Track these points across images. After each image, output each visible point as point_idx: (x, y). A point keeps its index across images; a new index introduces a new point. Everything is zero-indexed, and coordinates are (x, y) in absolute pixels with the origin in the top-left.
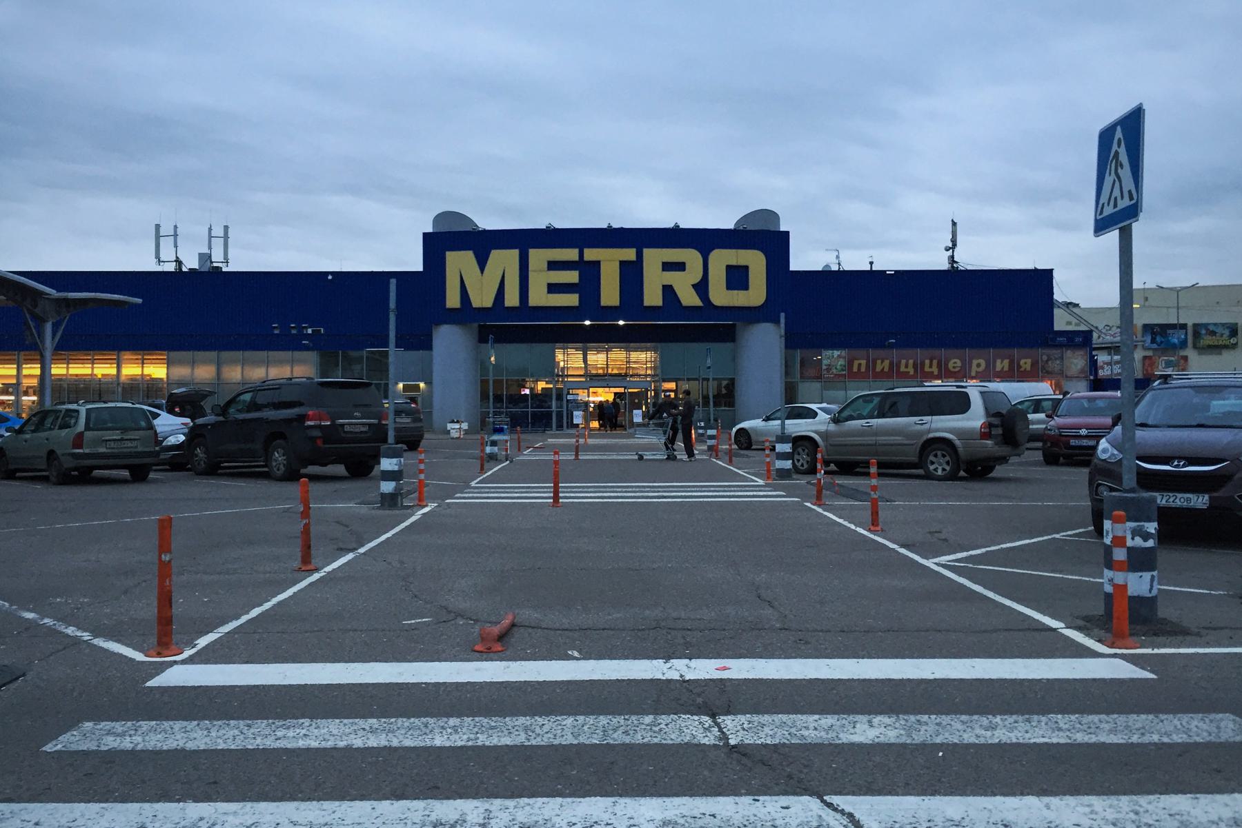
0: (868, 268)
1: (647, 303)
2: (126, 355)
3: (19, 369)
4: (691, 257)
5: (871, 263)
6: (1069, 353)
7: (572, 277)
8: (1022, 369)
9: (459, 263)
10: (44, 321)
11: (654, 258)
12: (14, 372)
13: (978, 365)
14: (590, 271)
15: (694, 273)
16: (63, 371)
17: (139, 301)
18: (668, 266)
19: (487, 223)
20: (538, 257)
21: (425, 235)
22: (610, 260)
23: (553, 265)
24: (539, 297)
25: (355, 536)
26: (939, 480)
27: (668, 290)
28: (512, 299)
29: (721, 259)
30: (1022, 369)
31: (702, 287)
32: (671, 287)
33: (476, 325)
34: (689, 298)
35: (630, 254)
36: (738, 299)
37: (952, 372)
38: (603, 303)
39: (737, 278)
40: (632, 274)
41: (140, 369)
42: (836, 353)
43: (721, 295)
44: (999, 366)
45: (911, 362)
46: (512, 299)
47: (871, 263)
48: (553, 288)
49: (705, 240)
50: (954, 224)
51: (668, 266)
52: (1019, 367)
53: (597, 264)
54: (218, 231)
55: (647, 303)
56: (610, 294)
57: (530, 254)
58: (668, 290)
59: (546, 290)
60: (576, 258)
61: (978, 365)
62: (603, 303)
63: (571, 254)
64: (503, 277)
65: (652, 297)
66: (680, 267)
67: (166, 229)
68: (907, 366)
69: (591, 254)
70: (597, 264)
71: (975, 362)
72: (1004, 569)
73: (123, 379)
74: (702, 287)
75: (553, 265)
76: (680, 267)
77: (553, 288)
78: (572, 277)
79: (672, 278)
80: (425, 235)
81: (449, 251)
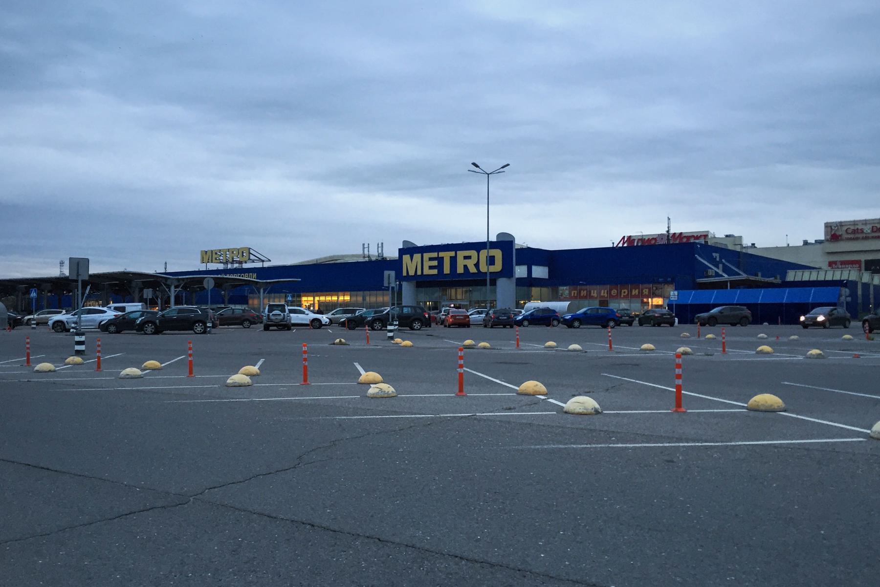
0: (612, 246)
1: (458, 272)
2: (340, 293)
3: (338, 298)
4: (473, 253)
5: (613, 243)
6: (666, 286)
7: (435, 263)
8: (644, 294)
9: (406, 258)
10: (260, 289)
11: (461, 254)
12: (337, 299)
13: (624, 292)
14: (441, 260)
15: (474, 260)
16: (330, 299)
17: (300, 280)
18: (466, 258)
19: (419, 244)
20: (427, 256)
21: (399, 249)
22: (447, 256)
23: (431, 259)
24: (427, 271)
25: (625, 390)
26: (111, 323)
27: (465, 267)
28: (419, 273)
29: (484, 254)
30: (644, 294)
31: (477, 265)
32: (466, 265)
33: (415, 281)
34: (473, 270)
35: (452, 254)
36: (492, 269)
37: (613, 296)
38: (444, 273)
39: (491, 261)
40: (453, 260)
41: (375, 298)
42: (565, 288)
43: (483, 268)
44: (634, 293)
45: (606, 291)
46: (419, 273)
47: (613, 243)
48: (431, 268)
49: (478, 247)
50: (669, 219)
51: (466, 258)
52: (642, 293)
53: (443, 258)
54: (380, 245)
55: (458, 272)
56: (447, 270)
57: (435, 253)
58: (465, 267)
59: (428, 268)
60: (437, 256)
61: (624, 292)
62: (444, 273)
63: (435, 255)
64: (417, 266)
65: (460, 270)
66: (469, 257)
67: (366, 246)
68: (604, 293)
69: (441, 254)
70: (443, 258)
71: (623, 291)
72: (701, 396)
73: (339, 301)
74: (477, 265)
75: (431, 259)
76: (469, 257)
77: (431, 268)
78: (435, 263)
79: (467, 262)
80: (399, 249)
81: (405, 255)
